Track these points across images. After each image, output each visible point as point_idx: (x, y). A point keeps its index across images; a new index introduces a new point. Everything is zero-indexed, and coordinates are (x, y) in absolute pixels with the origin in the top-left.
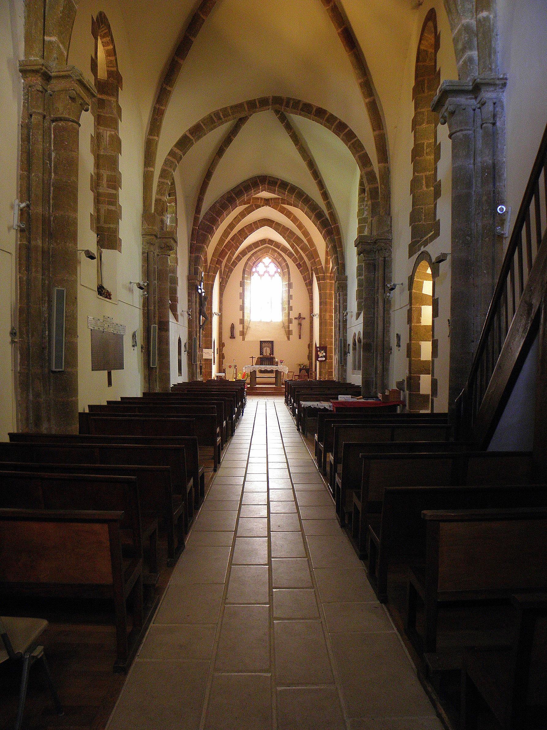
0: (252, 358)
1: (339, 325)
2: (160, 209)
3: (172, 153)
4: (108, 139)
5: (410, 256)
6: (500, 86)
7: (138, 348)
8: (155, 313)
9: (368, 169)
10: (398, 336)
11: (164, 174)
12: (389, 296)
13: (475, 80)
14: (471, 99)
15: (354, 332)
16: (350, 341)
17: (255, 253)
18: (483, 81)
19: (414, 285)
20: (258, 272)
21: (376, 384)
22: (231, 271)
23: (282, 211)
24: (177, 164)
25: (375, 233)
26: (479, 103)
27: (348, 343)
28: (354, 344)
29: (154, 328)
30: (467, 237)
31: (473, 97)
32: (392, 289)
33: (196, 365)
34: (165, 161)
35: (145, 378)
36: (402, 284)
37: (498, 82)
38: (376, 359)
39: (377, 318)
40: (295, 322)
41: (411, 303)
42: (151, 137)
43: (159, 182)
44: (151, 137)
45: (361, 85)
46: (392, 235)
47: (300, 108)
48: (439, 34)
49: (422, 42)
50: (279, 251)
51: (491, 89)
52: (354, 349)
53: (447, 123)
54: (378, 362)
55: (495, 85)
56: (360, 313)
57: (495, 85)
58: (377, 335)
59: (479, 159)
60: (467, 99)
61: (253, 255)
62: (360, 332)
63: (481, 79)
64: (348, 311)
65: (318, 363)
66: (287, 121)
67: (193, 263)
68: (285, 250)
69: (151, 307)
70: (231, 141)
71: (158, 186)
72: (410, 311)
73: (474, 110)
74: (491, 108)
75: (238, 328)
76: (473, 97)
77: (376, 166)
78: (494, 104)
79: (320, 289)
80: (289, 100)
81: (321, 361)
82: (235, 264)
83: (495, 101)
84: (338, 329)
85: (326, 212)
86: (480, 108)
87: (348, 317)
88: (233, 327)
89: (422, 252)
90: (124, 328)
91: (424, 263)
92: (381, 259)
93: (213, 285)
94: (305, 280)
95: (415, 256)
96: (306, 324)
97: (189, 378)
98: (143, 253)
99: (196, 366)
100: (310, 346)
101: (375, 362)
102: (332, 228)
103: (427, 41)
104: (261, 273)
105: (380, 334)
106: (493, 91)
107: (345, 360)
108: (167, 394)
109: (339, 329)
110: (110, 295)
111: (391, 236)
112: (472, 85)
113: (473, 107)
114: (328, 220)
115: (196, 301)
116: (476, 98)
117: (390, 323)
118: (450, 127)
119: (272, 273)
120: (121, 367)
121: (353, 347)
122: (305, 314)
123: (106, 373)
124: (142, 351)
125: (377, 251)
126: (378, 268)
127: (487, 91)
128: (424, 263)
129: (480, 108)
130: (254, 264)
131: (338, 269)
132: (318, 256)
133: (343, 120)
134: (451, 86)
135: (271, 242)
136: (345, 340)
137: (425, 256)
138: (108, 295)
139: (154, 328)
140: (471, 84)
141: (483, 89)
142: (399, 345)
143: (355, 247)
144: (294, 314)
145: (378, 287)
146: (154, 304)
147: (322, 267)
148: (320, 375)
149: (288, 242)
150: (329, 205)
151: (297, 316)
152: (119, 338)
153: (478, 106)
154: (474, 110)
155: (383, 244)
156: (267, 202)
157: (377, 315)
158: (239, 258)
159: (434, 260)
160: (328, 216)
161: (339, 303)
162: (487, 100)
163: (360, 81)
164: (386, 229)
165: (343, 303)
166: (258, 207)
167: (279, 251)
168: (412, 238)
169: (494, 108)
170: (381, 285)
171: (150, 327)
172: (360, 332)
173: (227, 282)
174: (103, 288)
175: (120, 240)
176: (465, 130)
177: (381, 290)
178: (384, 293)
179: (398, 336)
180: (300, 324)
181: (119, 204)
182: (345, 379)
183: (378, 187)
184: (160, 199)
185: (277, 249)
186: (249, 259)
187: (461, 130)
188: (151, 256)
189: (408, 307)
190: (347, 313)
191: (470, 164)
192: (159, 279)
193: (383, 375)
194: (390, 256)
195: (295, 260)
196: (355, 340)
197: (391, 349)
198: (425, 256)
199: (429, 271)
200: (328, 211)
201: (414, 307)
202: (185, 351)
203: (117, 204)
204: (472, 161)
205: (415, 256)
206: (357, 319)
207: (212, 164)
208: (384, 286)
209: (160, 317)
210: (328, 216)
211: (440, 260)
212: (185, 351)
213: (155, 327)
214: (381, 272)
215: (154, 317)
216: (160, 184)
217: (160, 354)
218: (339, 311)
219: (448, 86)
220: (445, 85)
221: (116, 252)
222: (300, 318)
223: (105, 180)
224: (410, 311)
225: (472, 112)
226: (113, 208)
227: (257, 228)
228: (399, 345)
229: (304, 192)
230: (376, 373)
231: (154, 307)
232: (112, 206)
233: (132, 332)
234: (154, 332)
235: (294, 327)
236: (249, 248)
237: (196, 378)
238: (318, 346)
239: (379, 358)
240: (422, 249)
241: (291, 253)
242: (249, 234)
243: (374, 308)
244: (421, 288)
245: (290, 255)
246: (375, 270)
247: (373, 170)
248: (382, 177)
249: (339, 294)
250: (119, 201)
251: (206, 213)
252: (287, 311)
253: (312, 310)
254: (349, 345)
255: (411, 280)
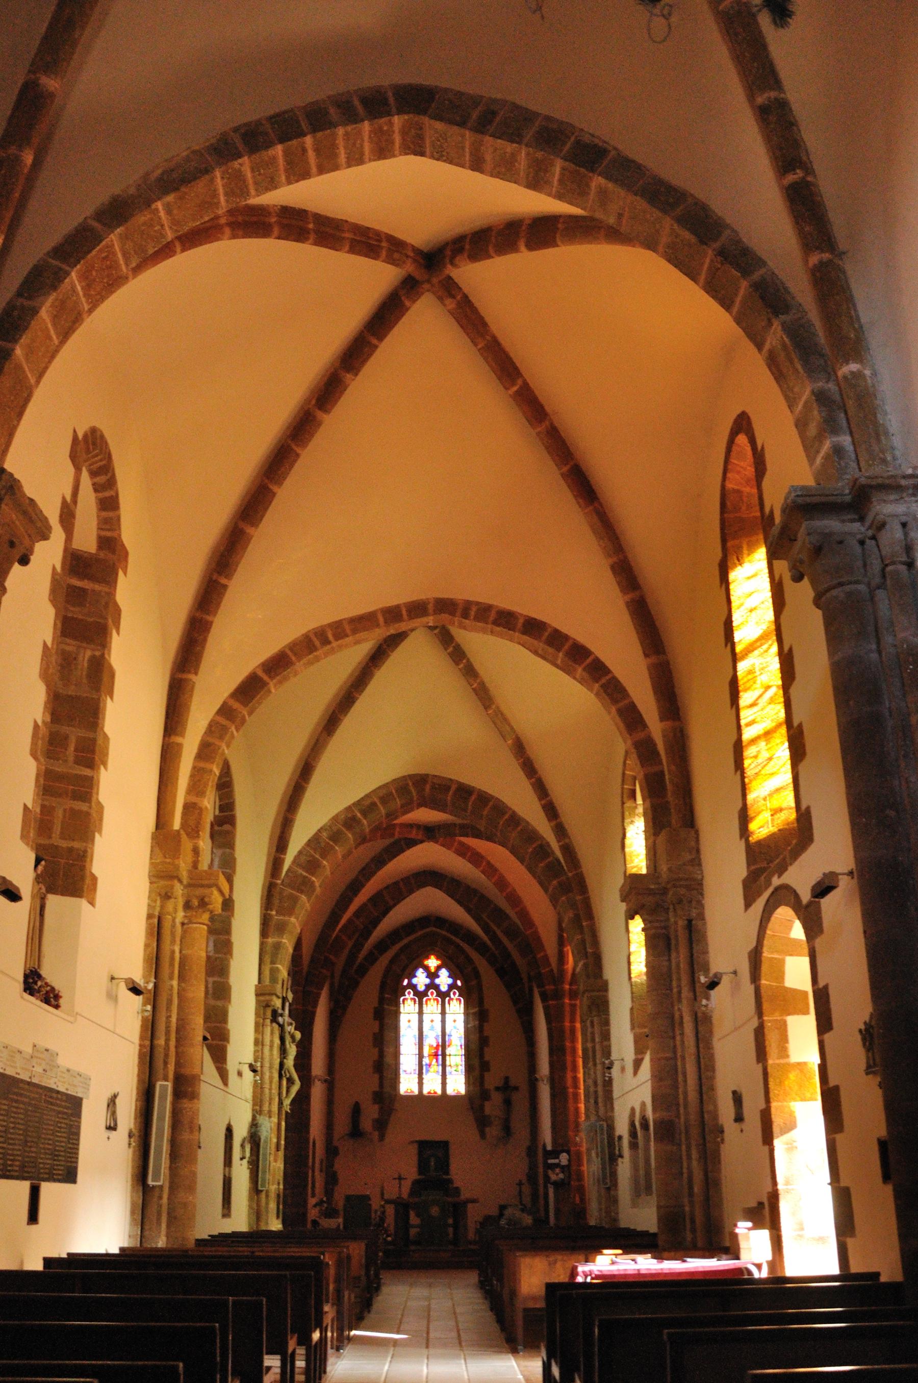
0: (400, 1178)
1: (596, 1092)
2: (192, 823)
3: (225, 711)
4: (86, 665)
5: (748, 904)
6: (911, 491)
7: (121, 1136)
8: (167, 1055)
9: (641, 735)
10: (737, 1098)
11: (206, 751)
12: (706, 1006)
13: (856, 480)
14: (852, 521)
15: (630, 1106)
16: (622, 1128)
17: (406, 946)
18: (874, 483)
19: (765, 968)
20: (414, 987)
21: (693, 1221)
22: (355, 984)
23: (464, 852)
24: (235, 733)
25: (664, 868)
26: (870, 527)
27: (617, 1133)
28: (633, 1134)
29: (164, 1088)
30: (888, 812)
31: (856, 517)
32: (713, 985)
33: (267, 1192)
34: (210, 726)
35: (133, 1213)
36: (735, 973)
37: (903, 482)
38: (689, 1157)
39: (683, 1058)
40: (497, 1098)
41: (760, 1012)
42: (180, 676)
43: (194, 768)
44: (180, 676)
45: (613, 568)
46: (702, 870)
47: (491, 619)
48: (763, 448)
49: (729, 475)
50: (458, 941)
51: (892, 497)
52: (634, 1145)
53: (806, 578)
54: (695, 1163)
55: (898, 488)
56: (642, 1059)
57: (898, 488)
58: (685, 1098)
59: (888, 639)
60: (843, 521)
61: (402, 950)
62: (643, 1104)
63: (869, 477)
64: (612, 1058)
65: (551, 1191)
66: (468, 660)
67: (267, 959)
68: (470, 937)
69: (159, 1038)
70: (353, 702)
71: (192, 776)
72: (760, 1034)
73: (862, 543)
74: (899, 534)
75: (371, 1112)
76: (856, 517)
77: (656, 727)
78: (904, 525)
79: (549, 1021)
80: (468, 605)
81: (556, 1184)
82: (363, 970)
83: (904, 519)
84: (592, 1101)
85: (555, 845)
86: (873, 538)
87: (615, 1072)
88: (356, 1110)
89: (777, 889)
90: (86, 1081)
91: (784, 913)
92: (681, 923)
93: (313, 1014)
94: (515, 1003)
95: (759, 904)
96: (520, 1101)
97: (250, 1224)
98: (150, 916)
99: (267, 1196)
100: (531, 1151)
101: (685, 1165)
102: (568, 879)
103: (738, 472)
104: (421, 988)
105: (692, 1095)
106: (897, 500)
107: (614, 1174)
108: (185, 1253)
109: (596, 1102)
110: (57, 997)
111: (698, 872)
112: (850, 493)
113: (859, 536)
114: (558, 860)
115: (272, 1042)
116: (862, 519)
117: (713, 1070)
118: (813, 583)
119: (444, 988)
120: (70, 1176)
121: (630, 1142)
122: (519, 1079)
123: (24, 1187)
124: (130, 1144)
125: (671, 907)
126: (677, 944)
127: (884, 501)
128: (784, 913)
129: (873, 538)
130: (404, 970)
131: (586, 966)
132: (542, 947)
133: (582, 639)
134: (806, 496)
135: (440, 921)
136: (611, 1128)
137: (785, 896)
138: (51, 998)
139: (164, 1088)
140: (847, 491)
141: (876, 497)
142: (739, 1118)
143: (622, 901)
144: (492, 1080)
145: (679, 986)
146: (168, 1033)
147: (552, 970)
148: (557, 1217)
149: (477, 919)
150: (560, 831)
151: (500, 1083)
152: (75, 1104)
153: (870, 533)
154: (862, 543)
155: (683, 891)
156: (430, 832)
157: (683, 1051)
158: (372, 958)
159: (806, 896)
160: (559, 854)
161: (593, 1040)
162: (887, 519)
163: (611, 561)
164: (688, 857)
165: (602, 1042)
166: (411, 843)
167: (458, 941)
168: (749, 864)
169: (906, 534)
170: (685, 981)
171: (154, 1086)
172: (643, 1104)
173: (345, 1008)
174: (40, 977)
175: (94, 879)
176: (850, 583)
177: (686, 993)
178: (695, 999)
179: (737, 1098)
180: (508, 1102)
181: (97, 799)
182: (616, 1220)
183: (662, 772)
184: (195, 804)
185: (453, 938)
186: (392, 961)
187: (841, 584)
188: (167, 925)
189: (755, 1023)
190: (612, 1063)
191: (871, 651)
192: (181, 978)
193: (707, 1199)
194: (702, 916)
195: (492, 961)
196: (632, 1124)
197: (722, 1132)
198: (785, 896)
199: (798, 931)
200: (559, 841)
201: (770, 1021)
202: (242, 1159)
203: (94, 800)
204: (874, 647)
205: (759, 904)
206: (635, 1073)
207: (312, 749)
208: (693, 981)
209: (178, 1064)
210: (559, 854)
211: (823, 889)
212: (242, 1159)
213: (164, 1087)
214: (683, 952)
215: (166, 1063)
216: (197, 774)
217: (174, 1155)
218: (594, 1060)
219: (802, 496)
220: (793, 494)
221: (84, 903)
222: (506, 1088)
223: (72, 748)
224: (760, 1034)
225: (858, 549)
226: (84, 807)
227: (411, 892)
228: (739, 1118)
229: (507, 807)
230: (691, 1194)
231: (167, 1040)
232: (80, 803)
233: (109, 1095)
234: (163, 1098)
235: (493, 1108)
236: (395, 935)
237: (267, 1223)
238: (549, 1148)
239: (695, 1154)
240: (776, 881)
241: (484, 944)
242: (391, 903)
243: (674, 1038)
244: (780, 974)
245: (482, 949)
246: (669, 949)
247: (649, 737)
248: (670, 749)
249: (592, 1022)
250: (97, 794)
251: (300, 852)
252: (477, 1073)
253: (532, 1067)
254: (620, 1138)
255: (755, 957)
